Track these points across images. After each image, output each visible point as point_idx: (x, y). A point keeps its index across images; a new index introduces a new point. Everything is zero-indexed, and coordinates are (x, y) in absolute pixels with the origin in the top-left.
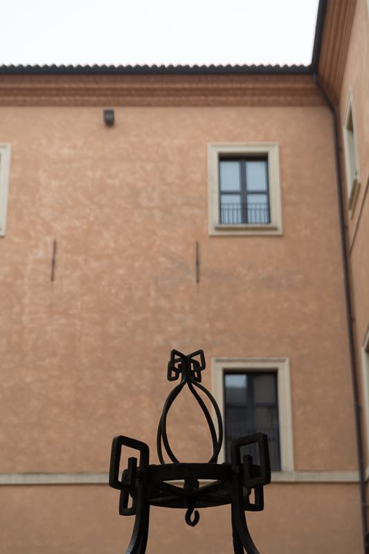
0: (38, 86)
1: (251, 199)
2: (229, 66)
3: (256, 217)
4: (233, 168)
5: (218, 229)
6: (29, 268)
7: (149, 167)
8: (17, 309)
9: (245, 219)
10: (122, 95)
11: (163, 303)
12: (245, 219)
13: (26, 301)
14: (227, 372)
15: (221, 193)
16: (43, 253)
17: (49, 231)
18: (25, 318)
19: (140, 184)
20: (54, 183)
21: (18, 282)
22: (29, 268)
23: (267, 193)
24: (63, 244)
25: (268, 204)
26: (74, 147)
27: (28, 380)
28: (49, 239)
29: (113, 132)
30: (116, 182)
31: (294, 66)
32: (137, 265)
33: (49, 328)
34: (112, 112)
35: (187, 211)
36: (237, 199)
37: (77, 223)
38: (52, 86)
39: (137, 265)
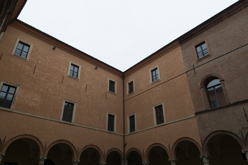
0: (87, 58)
1: (74, 73)
2: (55, 38)
3: (23, 55)
4: (21, 45)
5: (69, 76)
6: (83, 88)
7: (100, 78)
8: (80, 94)
9: (20, 55)
10: (23, 29)
11: (101, 100)
12: (20, 55)
13: (82, 94)
14: (4, 84)
15: (17, 49)
16: (85, 86)
17: (86, 83)
18: (81, 97)
19: (99, 80)
20: (87, 75)
21: (81, 90)
22: (83, 88)
23: (27, 53)
24: (88, 86)
25: (27, 55)
26: (90, 70)
27: (81, 107)
28: (86, 84)
29: (52, 50)
30: (96, 78)
31: (30, 25)
32: (98, 93)
33: (85, 99)
34: (97, 67)
35: (105, 87)
36: (20, 51)
37: (90, 83)
38: (89, 59)
39: (98, 93)
